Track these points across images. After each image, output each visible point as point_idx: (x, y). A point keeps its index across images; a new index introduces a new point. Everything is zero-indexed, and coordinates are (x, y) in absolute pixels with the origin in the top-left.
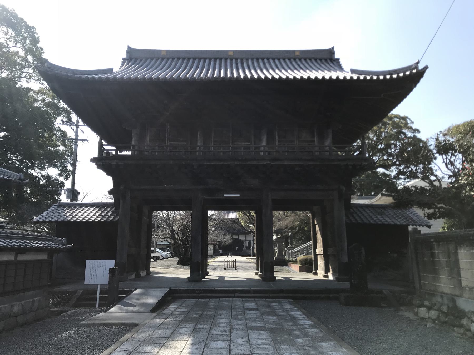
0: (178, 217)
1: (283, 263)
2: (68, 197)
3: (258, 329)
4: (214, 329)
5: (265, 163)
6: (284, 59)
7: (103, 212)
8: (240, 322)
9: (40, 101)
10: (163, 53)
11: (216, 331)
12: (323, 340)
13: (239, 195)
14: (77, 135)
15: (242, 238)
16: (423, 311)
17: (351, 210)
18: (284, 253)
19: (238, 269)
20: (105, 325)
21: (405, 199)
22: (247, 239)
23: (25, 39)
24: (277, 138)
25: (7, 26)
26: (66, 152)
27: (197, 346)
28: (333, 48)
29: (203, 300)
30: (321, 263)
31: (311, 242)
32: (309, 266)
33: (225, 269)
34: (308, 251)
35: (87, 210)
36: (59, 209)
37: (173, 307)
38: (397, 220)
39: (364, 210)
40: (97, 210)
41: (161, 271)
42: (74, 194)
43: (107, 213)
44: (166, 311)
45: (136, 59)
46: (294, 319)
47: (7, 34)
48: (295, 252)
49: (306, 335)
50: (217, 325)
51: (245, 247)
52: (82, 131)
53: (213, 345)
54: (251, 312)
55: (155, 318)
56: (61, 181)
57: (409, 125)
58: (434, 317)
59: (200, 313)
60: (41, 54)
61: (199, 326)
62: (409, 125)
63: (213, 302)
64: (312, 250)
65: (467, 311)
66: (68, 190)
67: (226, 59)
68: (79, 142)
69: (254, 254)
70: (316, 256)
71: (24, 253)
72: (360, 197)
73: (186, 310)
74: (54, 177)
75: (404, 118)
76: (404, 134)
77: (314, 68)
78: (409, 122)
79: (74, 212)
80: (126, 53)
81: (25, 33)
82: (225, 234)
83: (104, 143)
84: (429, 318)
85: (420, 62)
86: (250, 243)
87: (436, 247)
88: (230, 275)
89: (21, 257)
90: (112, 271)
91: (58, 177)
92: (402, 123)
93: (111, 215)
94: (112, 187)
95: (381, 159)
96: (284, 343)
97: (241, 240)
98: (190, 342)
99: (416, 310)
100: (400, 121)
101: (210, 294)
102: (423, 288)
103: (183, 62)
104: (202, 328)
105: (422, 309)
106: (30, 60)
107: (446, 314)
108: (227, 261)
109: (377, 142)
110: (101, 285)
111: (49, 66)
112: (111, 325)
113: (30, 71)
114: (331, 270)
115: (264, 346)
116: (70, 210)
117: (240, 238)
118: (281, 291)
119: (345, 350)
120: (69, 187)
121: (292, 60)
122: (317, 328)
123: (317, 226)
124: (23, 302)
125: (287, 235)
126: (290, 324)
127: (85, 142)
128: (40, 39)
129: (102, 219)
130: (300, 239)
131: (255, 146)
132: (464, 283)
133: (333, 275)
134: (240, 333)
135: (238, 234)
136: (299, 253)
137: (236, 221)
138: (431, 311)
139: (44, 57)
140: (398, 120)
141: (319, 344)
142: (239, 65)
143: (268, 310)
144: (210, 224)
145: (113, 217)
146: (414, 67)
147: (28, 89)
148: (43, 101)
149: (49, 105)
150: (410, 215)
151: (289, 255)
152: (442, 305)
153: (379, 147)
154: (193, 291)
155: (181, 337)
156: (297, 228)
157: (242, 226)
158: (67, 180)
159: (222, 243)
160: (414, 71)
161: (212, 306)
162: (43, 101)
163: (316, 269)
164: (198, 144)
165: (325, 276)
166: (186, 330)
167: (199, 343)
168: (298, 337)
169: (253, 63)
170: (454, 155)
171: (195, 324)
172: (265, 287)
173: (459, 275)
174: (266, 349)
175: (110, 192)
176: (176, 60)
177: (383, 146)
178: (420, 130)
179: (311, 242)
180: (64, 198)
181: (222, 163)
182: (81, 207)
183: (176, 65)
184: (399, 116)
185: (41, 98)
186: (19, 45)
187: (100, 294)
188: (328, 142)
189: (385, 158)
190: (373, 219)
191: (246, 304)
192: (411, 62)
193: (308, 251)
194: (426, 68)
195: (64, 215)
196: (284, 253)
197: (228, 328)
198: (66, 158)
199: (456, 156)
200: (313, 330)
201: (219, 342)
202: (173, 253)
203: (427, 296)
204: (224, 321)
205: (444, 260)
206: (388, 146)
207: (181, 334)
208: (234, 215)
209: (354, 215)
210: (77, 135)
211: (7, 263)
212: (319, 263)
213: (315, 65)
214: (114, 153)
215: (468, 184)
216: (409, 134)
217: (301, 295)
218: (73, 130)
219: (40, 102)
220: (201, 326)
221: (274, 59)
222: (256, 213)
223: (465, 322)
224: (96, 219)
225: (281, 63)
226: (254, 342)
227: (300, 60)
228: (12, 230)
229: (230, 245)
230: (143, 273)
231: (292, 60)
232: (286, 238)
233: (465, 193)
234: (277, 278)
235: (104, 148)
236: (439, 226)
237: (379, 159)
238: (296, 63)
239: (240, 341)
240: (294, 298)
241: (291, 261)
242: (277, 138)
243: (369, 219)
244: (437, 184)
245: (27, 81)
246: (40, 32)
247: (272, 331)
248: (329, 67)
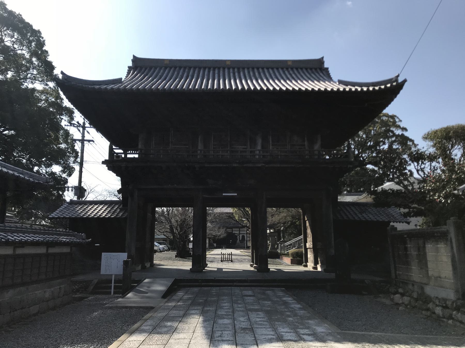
0: (176, 212)
1: (277, 256)
2: (75, 194)
3: (256, 310)
4: (219, 310)
5: (260, 165)
6: (277, 69)
7: (111, 209)
8: (240, 306)
9: (43, 100)
10: (166, 62)
11: (221, 312)
12: (309, 318)
13: (236, 194)
14: (83, 136)
15: (236, 232)
16: (397, 297)
18: (276, 246)
19: (234, 261)
20: (126, 307)
21: (385, 199)
22: (241, 232)
23: (30, 42)
24: (271, 142)
25: (13, 30)
26: (68, 149)
27: (208, 323)
28: (323, 58)
29: (206, 288)
30: (310, 256)
31: (302, 237)
32: (299, 259)
33: (222, 261)
34: (299, 244)
35: (97, 207)
36: (71, 206)
37: (180, 294)
38: (379, 217)
39: (350, 208)
40: (106, 207)
41: (162, 263)
42: (80, 191)
43: (115, 210)
44: (174, 297)
45: (141, 68)
46: (286, 304)
47: (12, 37)
48: (287, 246)
49: (296, 315)
50: (222, 308)
51: (238, 241)
52: (88, 132)
53: (221, 321)
54: (248, 298)
55: (166, 302)
56: (64, 178)
57: (397, 123)
58: (406, 303)
59: (205, 298)
60: (46, 57)
61: (206, 309)
62: (397, 123)
63: (214, 290)
64: (303, 244)
65: (433, 296)
66: (75, 188)
67: (224, 68)
68: (85, 142)
69: (248, 248)
70: (306, 249)
71: (54, 247)
72: (350, 193)
73: (192, 296)
74: (58, 173)
75: (393, 117)
76: (392, 132)
77: (305, 78)
78: (397, 120)
79: (85, 209)
80: (131, 62)
81: (30, 36)
82: (219, 228)
84: (403, 303)
85: (400, 76)
86: (243, 237)
87: (408, 242)
88: (227, 267)
89: (51, 250)
90: (125, 263)
91: (61, 173)
92: (390, 121)
93: (119, 212)
94: (120, 187)
95: (370, 156)
96: (278, 320)
97: (235, 234)
98: (201, 319)
99: (392, 297)
100: (388, 120)
101: (211, 284)
102: (398, 277)
103: (184, 71)
104: (209, 310)
105: (397, 295)
106: (35, 62)
107: (416, 300)
108: (224, 254)
109: (366, 140)
110: (116, 275)
111: (66, 78)
112: (131, 307)
113: (35, 72)
114: (319, 262)
115: (262, 322)
116: (81, 207)
117: (234, 232)
118: (274, 281)
119: (326, 325)
120: (76, 184)
121: (285, 69)
122: (305, 310)
123: (307, 222)
124: (52, 289)
125: (280, 230)
126: (283, 307)
127: (91, 142)
128: (46, 43)
129: (111, 215)
130: (292, 233)
131: (251, 150)
132: (430, 273)
133: (321, 266)
134: (241, 313)
135: (232, 228)
136: (290, 245)
137: (230, 216)
138: (404, 297)
139: (48, 60)
140: (387, 118)
141: (306, 321)
142: (236, 74)
143: (263, 297)
144: (209, 218)
145: (122, 213)
146: (394, 80)
147: (34, 90)
148: (46, 100)
149: (52, 104)
150: (392, 212)
151: (281, 248)
152: (413, 292)
153: (369, 144)
154: (196, 281)
155: (193, 316)
156: (289, 223)
157: (236, 221)
158: (70, 176)
159: (216, 236)
160: (394, 84)
161: (214, 293)
162: (46, 100)
163: (307, 261)
164: (199, 148)
165: (314, 268)
166: (196, 311)
167: (209, 320)
168: (289, 316)
169: (249, 73)
170: (424, 164)
171: (202, 307)
172: (260, 276)
173: (427, 267)
174: (264, 324)
175: (119, 191)
176: (177, 69)
177: (372, 143)
178: (407, 129)
179: (302, 237)
180: (69, 196)
182: (96, 204)
183: (178, 74)
184: (388, 114)
185: (44, 97)
186: (24, 48)
187: (114, 283)
188: (317, 147)
189: (374, 155)
190: (358, 216)
191: (243, 292)
192: (391, 76)
193: (299, 244)
194: (405, 81)
195: (76, 212)
196: (276, 246)
197: (230, 310)
198: (68, 155)
199: (425, 164)
200: (301, 312)
201: (225, 320)
202: (169, 246)
203: (401, 284)
204: (226, 304)
205: (415, 253)
206: (377, 144)
207: (193, 314)
208: (229, 210)
210: (83, 136)
211: (5, 257)
212: (309, 256)
213: (306, 75)
214: (123, 156)
215: (432, 190)
216: (399, 132)
217: (294, 284)
218: (79, 131)
219: (43, 102)
220: (208, 309)
221: (268, 69)
222: (251, 210)
223: (431, 306)
224: (106, 215)
225: (274, 72)
226: (253, 320)
227: (292, 69)
228: (16, 224)
229: (224, 239)
230: (148, 265)
231: (285, 69)
232: (278, 232)
233: (430, 197)
234: (271, 270)
235: (114, 152)
236: (416, 223)
237: (368, 156)
238: (289, 72)
239: (242, 319)
241: (285, 255)
242: (271, 142)
243: (354, 216)
244: (410, 188)
245: (32, 82)
246: (45, 35)
247: (268, 313)
248: (319, 76)
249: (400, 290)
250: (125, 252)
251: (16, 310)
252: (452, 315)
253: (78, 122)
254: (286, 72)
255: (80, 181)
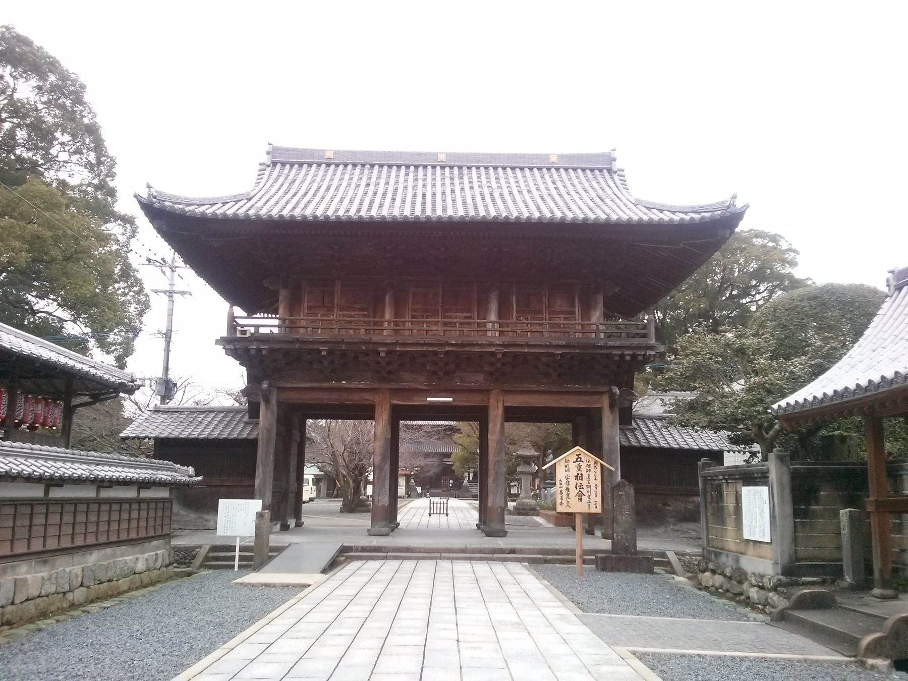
17: (633, 424)
83: (238, 311)
90: (260, 516)
103: (362, 172)
173: (69, 434)
181: (425, 349)
188: (597, 316)
209: (638, 433)
230: (292, 523)
240: (532, 561)
249: (711, 566)
250: (251, 496)
251: (101, 583)
252: (767, 599)
253: (163, 259)
254: (547, 177)
255: (166, 369)
